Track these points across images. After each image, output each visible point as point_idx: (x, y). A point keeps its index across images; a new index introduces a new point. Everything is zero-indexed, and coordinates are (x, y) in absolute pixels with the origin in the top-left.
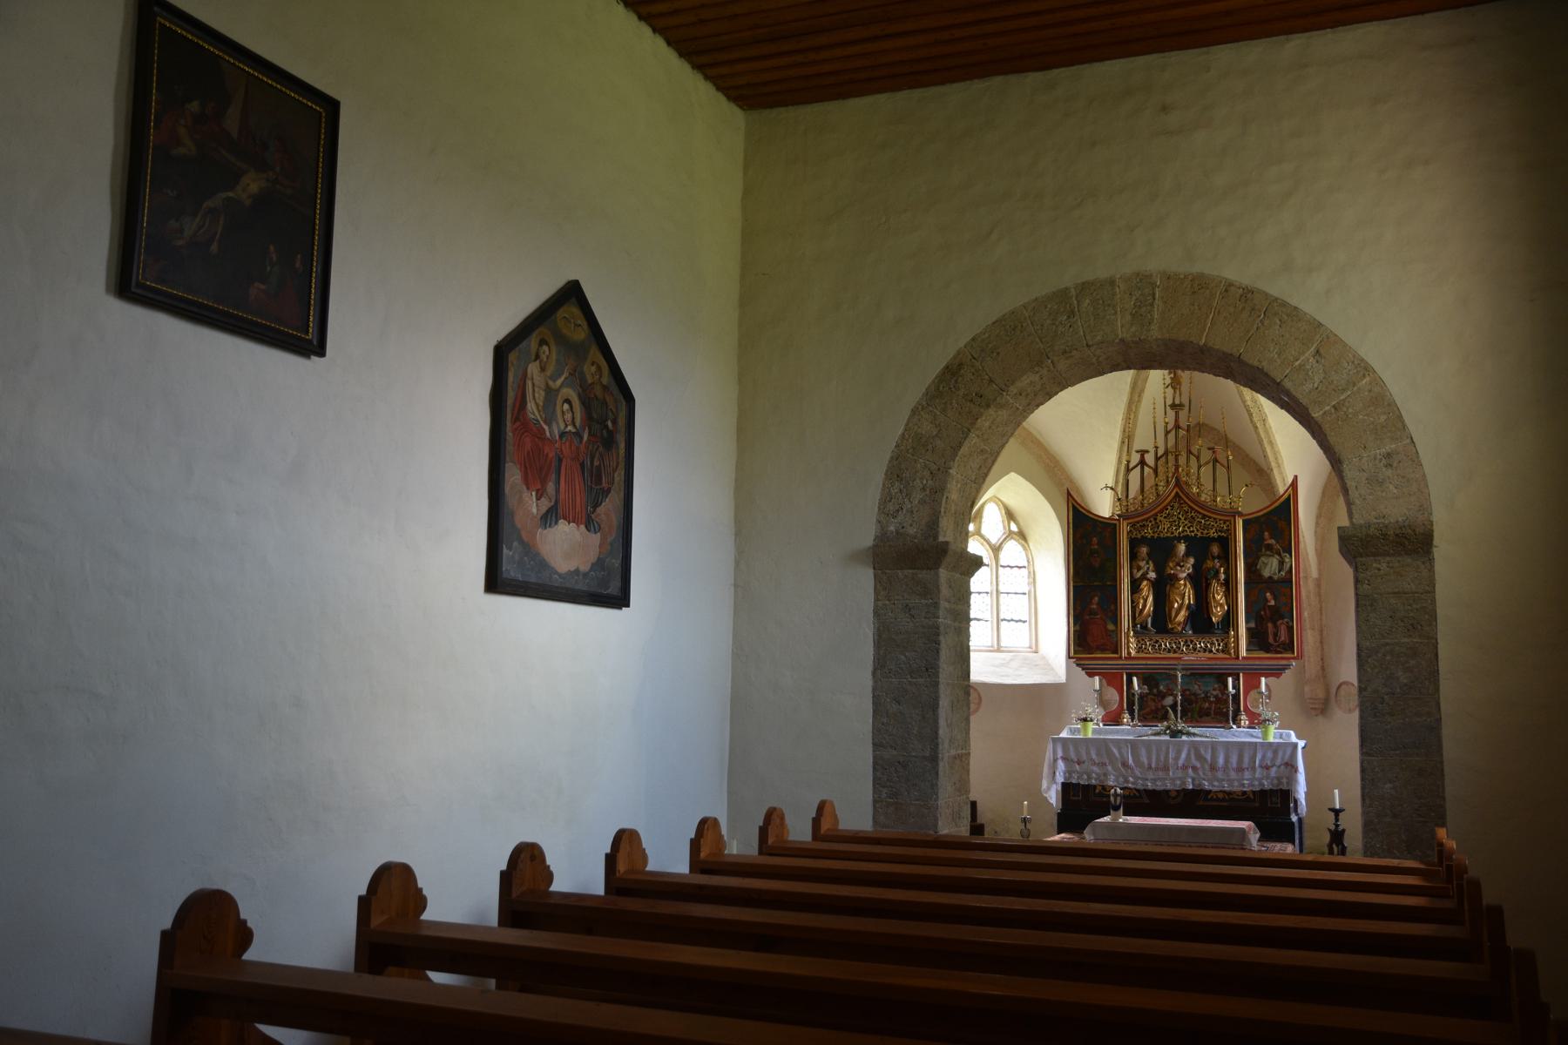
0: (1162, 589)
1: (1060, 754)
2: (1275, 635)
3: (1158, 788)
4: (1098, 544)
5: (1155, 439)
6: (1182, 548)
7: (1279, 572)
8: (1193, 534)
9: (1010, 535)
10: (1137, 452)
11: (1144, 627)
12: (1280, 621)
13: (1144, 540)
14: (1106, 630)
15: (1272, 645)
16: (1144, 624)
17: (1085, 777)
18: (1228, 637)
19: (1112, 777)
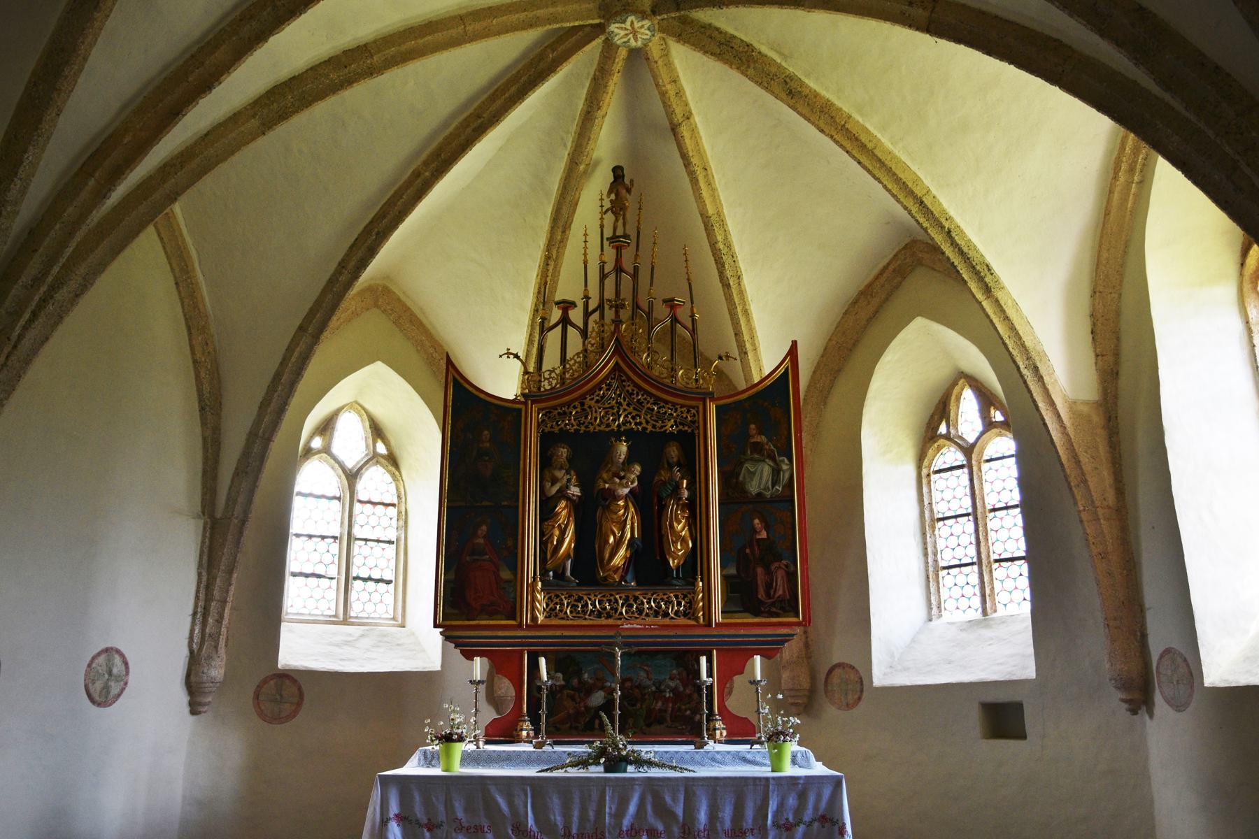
1: (394, 809)
2: (769, 586)
6: (623, 448)
7: (773, 486)
8: (640, 428)
9: (373, 458)
11: (560, 575)
12: (776, 564)
13: (564, 437)
18: (695, 592)
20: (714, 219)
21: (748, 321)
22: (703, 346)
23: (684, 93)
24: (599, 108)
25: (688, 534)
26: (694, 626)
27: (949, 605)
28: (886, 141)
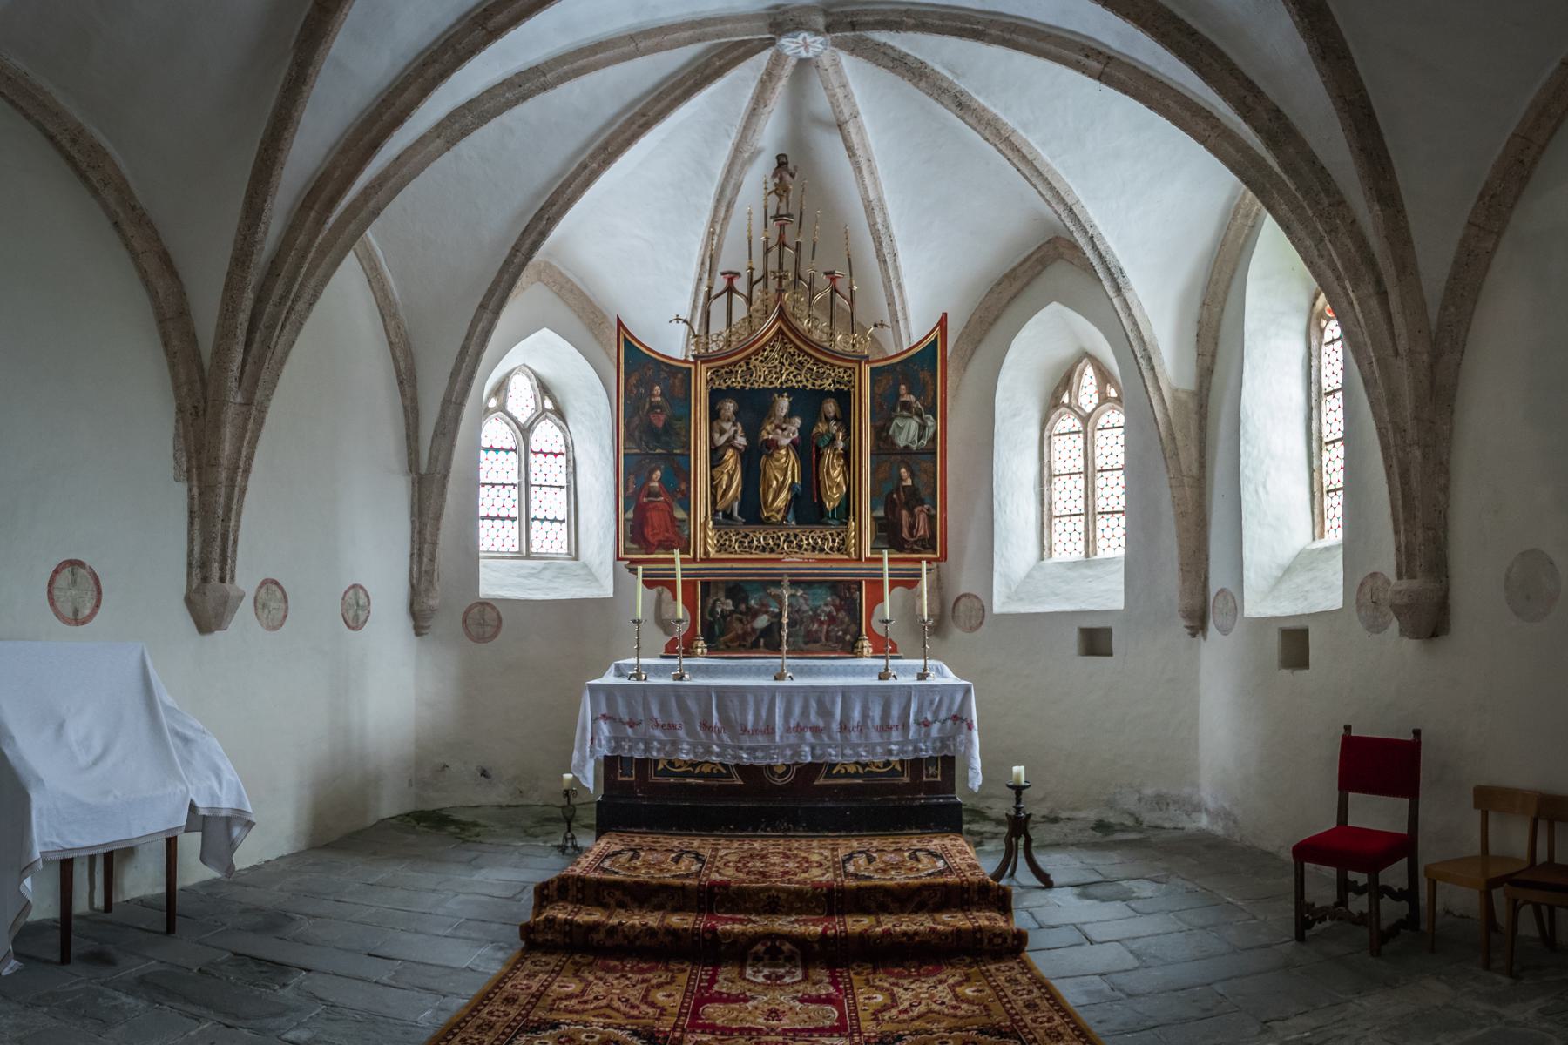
0: (755, 457)
2: (912, 527)
3: (757, 763)
4: (661, 395)
5: (750, 258)
6: (784, 404)
7: (919, 440)
8: (801, 386)
9: (541, 414)
10: (723, 274)
11: (728, 515)
12: (919, 508)
13: (730, 393)
14: (673, 519)
15: (906, 541)
16: (729, 512)
17: (641, 746)
19: (685, 746)
20: (874, 203)
21: (901, 293)
22: (859, 318)
23: (853, 95)
24: (766, 106)
25: (842, 480)
26: (846, 560)
27: (1058, 547)
28: (1045, 155)
